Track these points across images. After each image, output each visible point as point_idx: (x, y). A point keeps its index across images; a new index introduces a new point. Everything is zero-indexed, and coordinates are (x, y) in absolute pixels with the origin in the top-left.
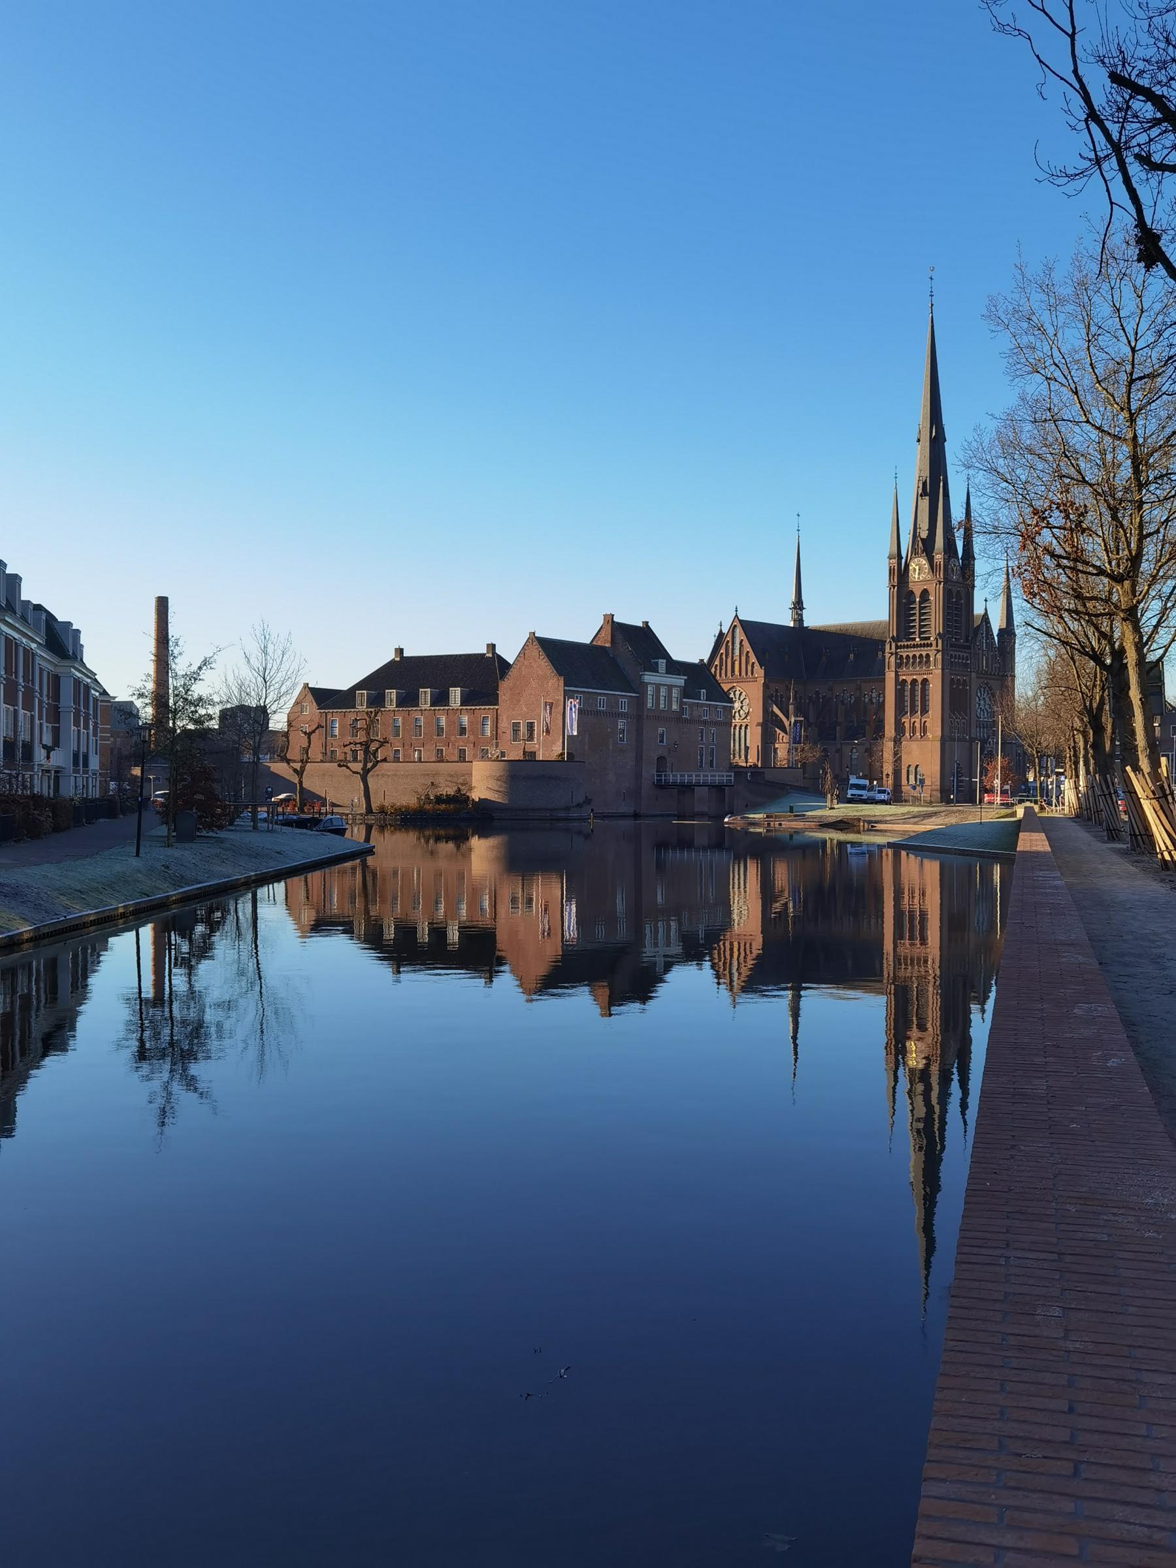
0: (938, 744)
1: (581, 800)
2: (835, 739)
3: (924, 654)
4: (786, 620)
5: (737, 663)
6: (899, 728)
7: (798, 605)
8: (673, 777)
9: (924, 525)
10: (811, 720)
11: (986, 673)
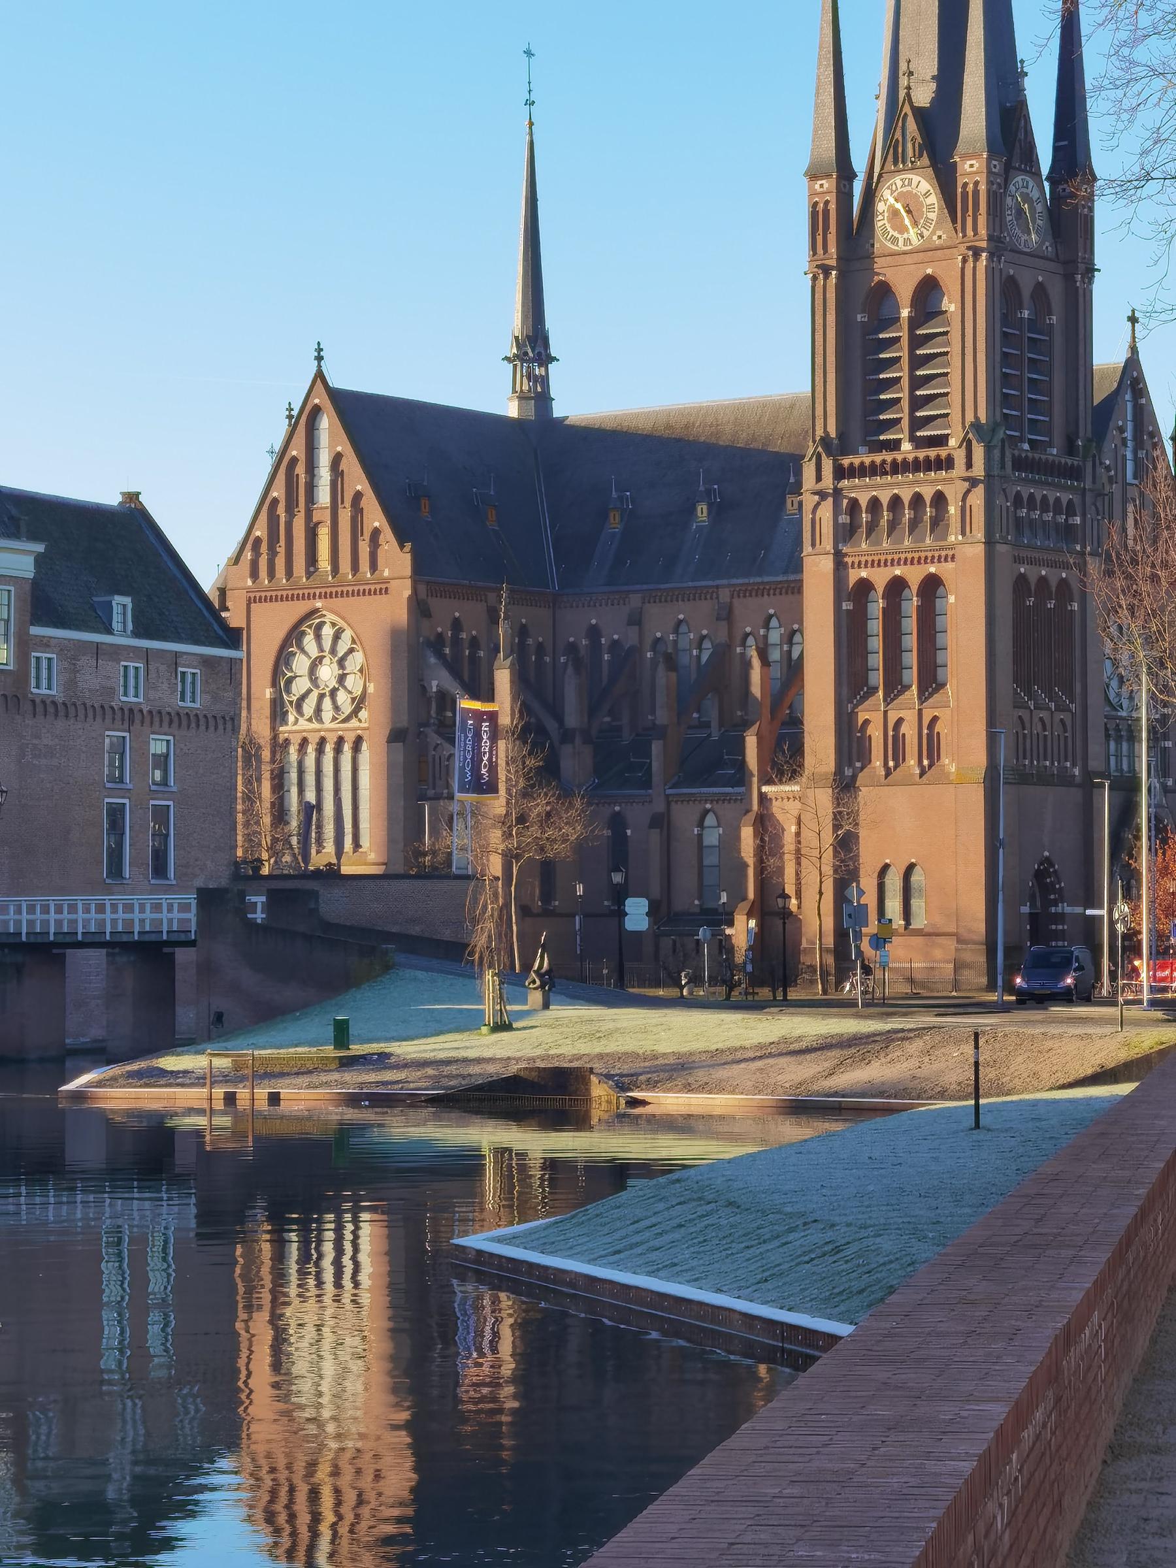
0: (977, 796)
2: (647, 784)
3: (928, 493)
4: (496, 396)
5: (324, 535)
6: (851, 746)
7: (534, 347)
9: (925, 63)
10: (572, 719)
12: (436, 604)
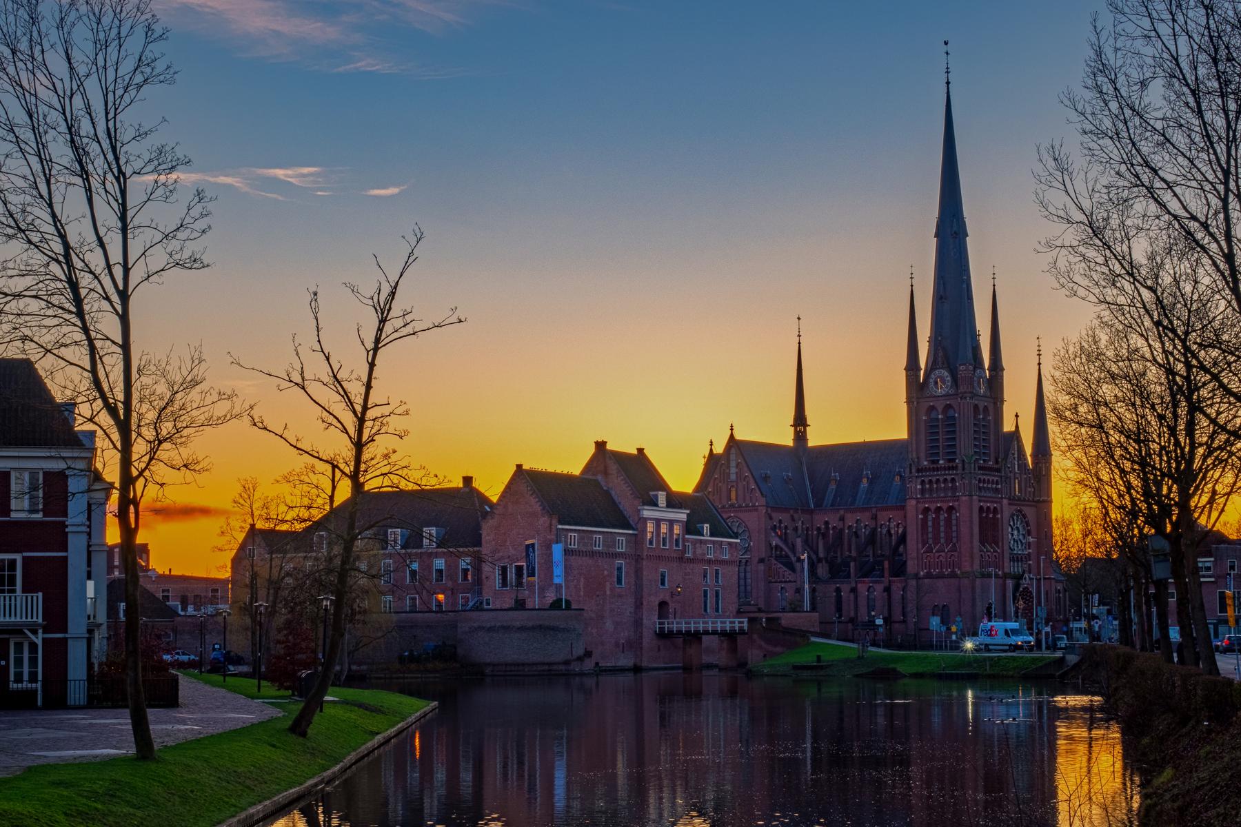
1: (581, 652)
2: (848, 576)
4: (786, 438)
7: (800, 420)
8: (676, 624)
10: (821, 555)
11: (1019, 499)
12: (774, 515)
